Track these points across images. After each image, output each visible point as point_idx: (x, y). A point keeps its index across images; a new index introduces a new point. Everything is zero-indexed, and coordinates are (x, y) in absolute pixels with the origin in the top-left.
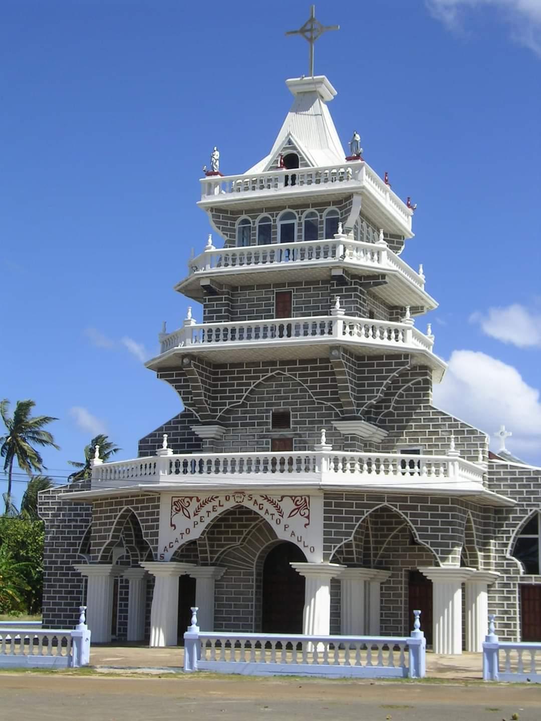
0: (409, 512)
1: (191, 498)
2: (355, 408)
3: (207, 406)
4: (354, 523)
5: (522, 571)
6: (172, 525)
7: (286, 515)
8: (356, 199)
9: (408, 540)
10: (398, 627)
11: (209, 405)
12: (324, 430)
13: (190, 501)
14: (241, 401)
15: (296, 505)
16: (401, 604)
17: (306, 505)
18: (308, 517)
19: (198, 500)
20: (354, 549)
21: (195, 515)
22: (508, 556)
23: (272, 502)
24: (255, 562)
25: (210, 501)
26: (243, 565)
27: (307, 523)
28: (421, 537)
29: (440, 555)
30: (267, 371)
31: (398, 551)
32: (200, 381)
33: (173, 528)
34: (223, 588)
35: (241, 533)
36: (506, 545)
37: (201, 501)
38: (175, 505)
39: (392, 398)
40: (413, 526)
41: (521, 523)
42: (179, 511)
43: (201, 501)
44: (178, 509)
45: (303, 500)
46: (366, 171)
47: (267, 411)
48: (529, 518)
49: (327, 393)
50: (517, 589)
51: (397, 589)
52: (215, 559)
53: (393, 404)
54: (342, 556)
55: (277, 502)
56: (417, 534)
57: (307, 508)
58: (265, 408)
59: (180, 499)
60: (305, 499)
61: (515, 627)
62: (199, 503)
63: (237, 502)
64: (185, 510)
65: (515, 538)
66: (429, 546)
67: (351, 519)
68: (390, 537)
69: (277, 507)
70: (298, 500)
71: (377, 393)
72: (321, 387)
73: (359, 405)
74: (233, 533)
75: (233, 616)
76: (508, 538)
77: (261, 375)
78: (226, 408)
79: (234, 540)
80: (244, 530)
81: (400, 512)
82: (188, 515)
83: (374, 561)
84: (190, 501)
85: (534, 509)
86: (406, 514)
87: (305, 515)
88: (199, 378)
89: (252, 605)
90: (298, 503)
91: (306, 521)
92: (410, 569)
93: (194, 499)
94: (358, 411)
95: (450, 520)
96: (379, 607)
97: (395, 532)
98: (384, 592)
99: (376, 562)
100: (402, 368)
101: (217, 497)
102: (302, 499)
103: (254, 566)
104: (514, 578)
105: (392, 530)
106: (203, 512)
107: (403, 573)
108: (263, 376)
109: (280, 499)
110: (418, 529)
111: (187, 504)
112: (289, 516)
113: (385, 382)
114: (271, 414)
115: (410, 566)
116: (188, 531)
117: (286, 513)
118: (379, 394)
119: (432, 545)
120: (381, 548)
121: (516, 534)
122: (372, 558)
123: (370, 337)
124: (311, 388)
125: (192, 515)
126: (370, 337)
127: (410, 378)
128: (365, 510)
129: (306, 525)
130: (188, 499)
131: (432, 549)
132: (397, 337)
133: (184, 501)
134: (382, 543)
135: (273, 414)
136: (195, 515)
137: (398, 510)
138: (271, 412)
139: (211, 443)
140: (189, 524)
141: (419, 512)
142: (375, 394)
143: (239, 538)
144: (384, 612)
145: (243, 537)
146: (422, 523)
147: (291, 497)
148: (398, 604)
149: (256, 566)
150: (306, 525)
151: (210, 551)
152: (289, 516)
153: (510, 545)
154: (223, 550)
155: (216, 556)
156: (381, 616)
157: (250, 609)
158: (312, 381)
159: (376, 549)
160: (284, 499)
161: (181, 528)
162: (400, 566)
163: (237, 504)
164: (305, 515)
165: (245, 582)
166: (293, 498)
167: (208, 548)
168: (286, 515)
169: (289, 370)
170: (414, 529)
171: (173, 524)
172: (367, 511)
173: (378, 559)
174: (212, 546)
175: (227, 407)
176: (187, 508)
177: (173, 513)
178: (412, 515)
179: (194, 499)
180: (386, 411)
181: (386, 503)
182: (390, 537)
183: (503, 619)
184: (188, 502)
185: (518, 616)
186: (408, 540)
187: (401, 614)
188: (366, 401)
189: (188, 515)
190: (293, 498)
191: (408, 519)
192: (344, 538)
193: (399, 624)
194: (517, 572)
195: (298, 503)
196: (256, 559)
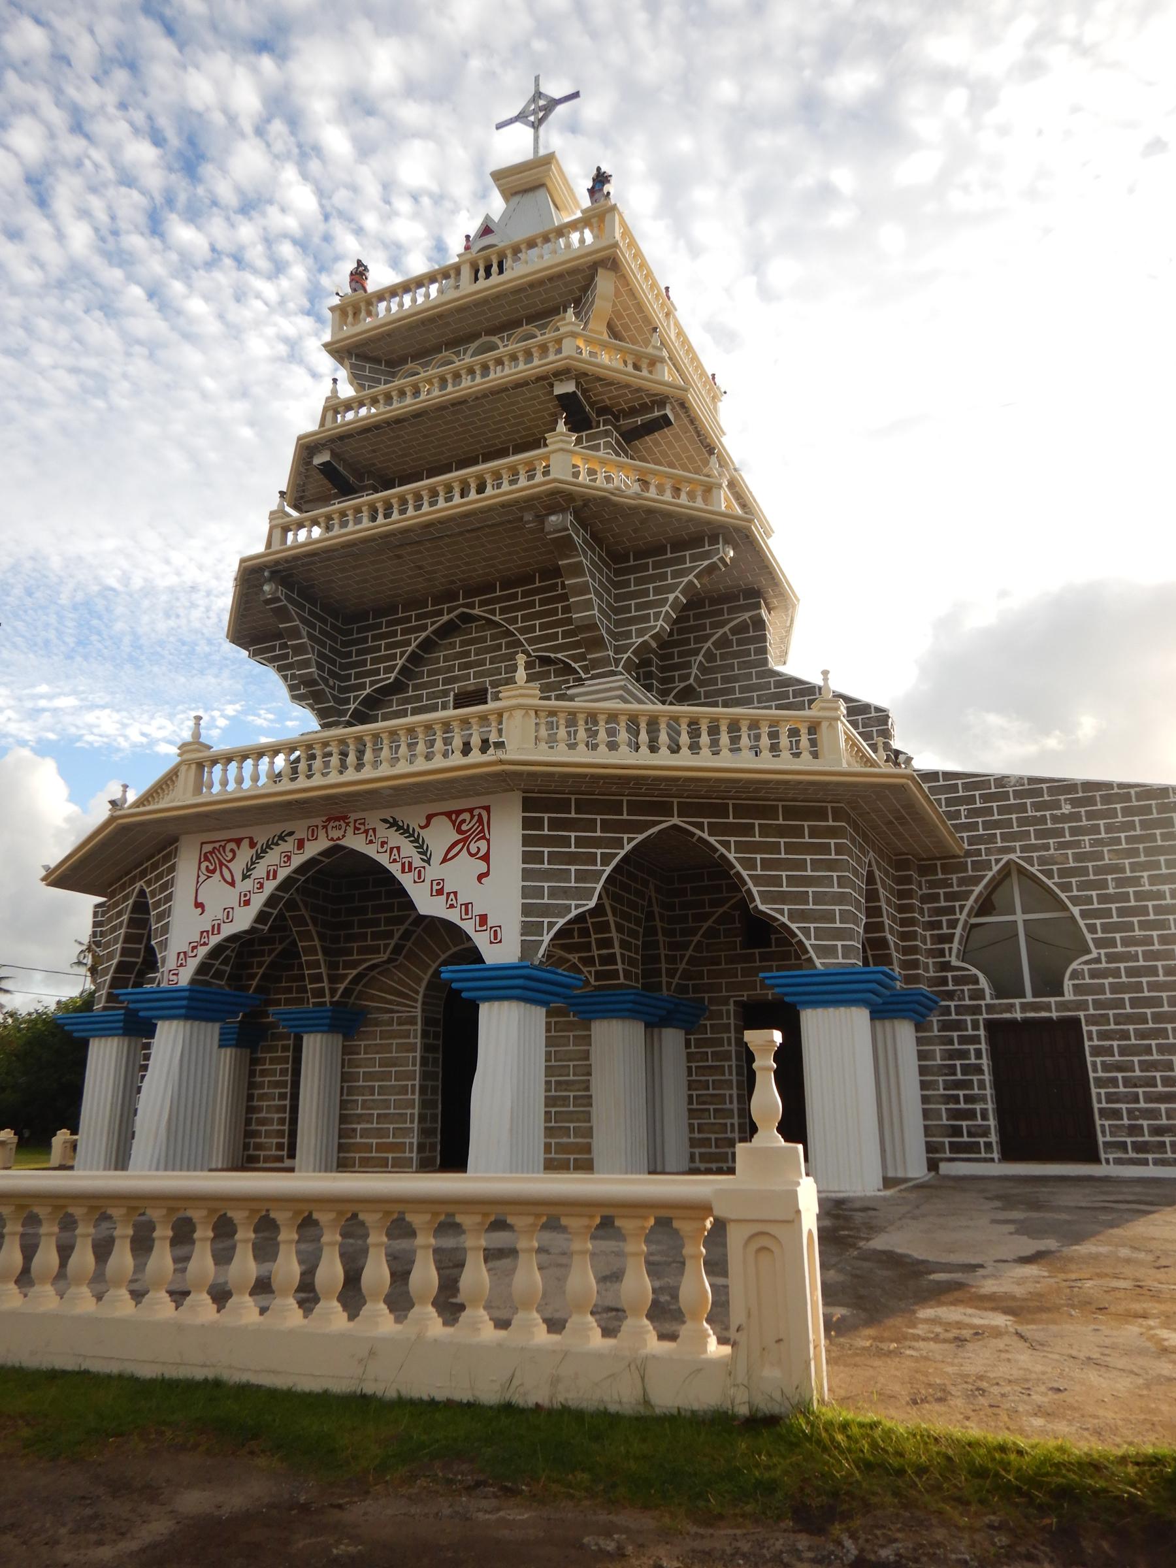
0: (732, 839)
1: (238, 842)
2: (611, 654)
3: (327, 690)
4: (599, 868)
5: (987, 992)
6: (198, 905)
7: (437, 857)
8: (604, 284)
9: (738, 939)
10: (726, 1124)
11: (333, 688)
12: (521, 659)
13: (236, 848)
14: (393, 675)
15: (459, 831)
16: (730, 1074)
17: (482, 831)
18: (486, 858)
19: (252, 845)
20: (617, 950)
21: (245, 877)
22: (955, 962)
23: (407, 831)
24: (421, 995)
25: (277, 844)
26: (399, 1004)
27: (485, 870)
28: (767, 898)
29: (813, 942)
30: (440, 613)
31: (719, 964)
32: (304, 633)
33: (199, 910)
34: (359, 1054)
35: (389, 935)
36: (949, 938)
37: (259, 846)
38: (206, 859)
39: (693, 659)
40: (744, 873)
41: (978, 889)
42: (213, 871)
43: (259, 846)
44: (211, 868)
45: (476, 818)
46: (620, 223)
47: (445, 693)
48: (994, 877)
49: (554, 636)
50: (982, 1032)
51: (720, 1042)
52: (340, 992)
53: (695, 671)
54: (593, 969)
55: (417, 829)
56: (754, 890)
57: (484, 838)
58: (441, 688)
59: (217, 845)
60: (480, 815)
61: (984, 1117)
62: (254, 851)
63: (332, 839)
64: (225, 870)
65: (966, 922)
66: (785, 920)
67: (592, 859)
68: (701, 933)
69: (416, 841)
70: (464, 821)
71: (656, 620)
72: (543, 627)
73: (618, 650)
74: (375, 936)
75: (375, 1112)
76: (953, 924)
77: (429, 621)
78: (366, 692)
79: (376, 950)
80: (395, 928)
81: (712, 840)
82: (229, 880)
83: (669, 984)
84: (236, 848)
85: (1006, 858)
86: (726, 845)
87: (480, 855)
88: (304, 630)
89: (413, 1086)
90: (464, 827)
91: (482, 867)
92: (745, 998)
93: (246, 843)
94: (617, 661)
95: (833, 857)
96: (686, 1084)
97: (710, 923)
98: (693, 1050)
99: (673, 987)
100: (706, 563)
101: (291, 834)
102: (472, 817)
103: (419, 1005)
104: (976, 1010)
105: (704, 917)
106: (260, 871)
107: (732, 1007)
108: (433, 623)
109: (423, 824)
110: (757, 880)
111: (230, 855)
112: (445, 860)
113: (671, 597)
114: (451, 698)
115: (745, 994)
116: (228, 912)
117: (438, 850)
118: (661, 622)
119: (793, 916)
120: (682, 957)
121: (969, 915)
122: (664, 979)
123: (685, 751)
124: (523, 631)
125: (238, 877)
126: (685, 751)
127: (726, 617)
128: (625, 836)
129: (480, 877)
130: (233, 845)
131: (793, 926)
132: (714, 743)
133: (224, 848)
134: (686, 946)
135: (456, 695)
136: (245, 877)
137: (705, 836)
138: (452, 694)
139: (744, 1109)
140: (231, 897)
141: (757, 839)
142: (652, 623)
143: (386, 946)
144: (694, 1093)
145: (393, 942)
146: (766, 864)
147: (448, 814)
148: (724, 1074)
149: (424, 1003)
150: (480, 877)
151: (328, 975)
152: (445, 860)
153: (956, 939)
154: (355, 972)
155: (342, 986)
156: (690, 1102)
157: (409, 1096)
158: (525, 618)
159: (671, 960)
160: (434, 821)
161: (214, 911)
162: (724, 994)
163: (332, 843)
164: (480, 855)
165: (401, 1038)
166: (454, 817)
167: (323, 970)
168: (437, 857)
169: (482, 604)
170: (747, 878)
171: (199, 901)
172: (630, 840)
173: (675, 981)
174: (332, 966)
175: (368, 691)
176: (229, 865)
177: (202, 878)
178: (740, 847)
179: (246, 843)
180: (682, 685)
181: (675, 820)
182: (701, 933)
183: (969, 1099)
184: (232, 851)
185: (989, 1092)
186: (738, 939)
187: (731, 1096)
188: (634, 640)
189: (229, 880)
190: (454, 817)
191: (731, 856)
192: (573, 903)
193: (728, 1118)
194: (978, 995)
195: (464, 827)
196: (422, 990)
